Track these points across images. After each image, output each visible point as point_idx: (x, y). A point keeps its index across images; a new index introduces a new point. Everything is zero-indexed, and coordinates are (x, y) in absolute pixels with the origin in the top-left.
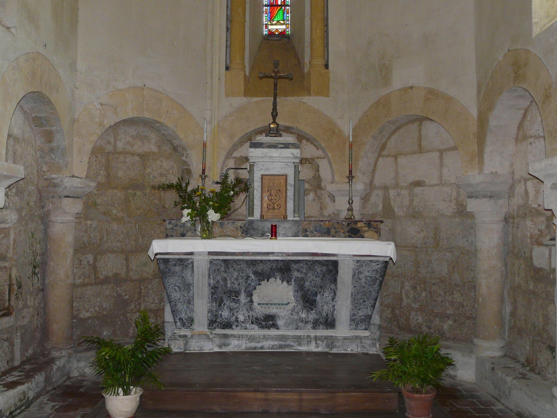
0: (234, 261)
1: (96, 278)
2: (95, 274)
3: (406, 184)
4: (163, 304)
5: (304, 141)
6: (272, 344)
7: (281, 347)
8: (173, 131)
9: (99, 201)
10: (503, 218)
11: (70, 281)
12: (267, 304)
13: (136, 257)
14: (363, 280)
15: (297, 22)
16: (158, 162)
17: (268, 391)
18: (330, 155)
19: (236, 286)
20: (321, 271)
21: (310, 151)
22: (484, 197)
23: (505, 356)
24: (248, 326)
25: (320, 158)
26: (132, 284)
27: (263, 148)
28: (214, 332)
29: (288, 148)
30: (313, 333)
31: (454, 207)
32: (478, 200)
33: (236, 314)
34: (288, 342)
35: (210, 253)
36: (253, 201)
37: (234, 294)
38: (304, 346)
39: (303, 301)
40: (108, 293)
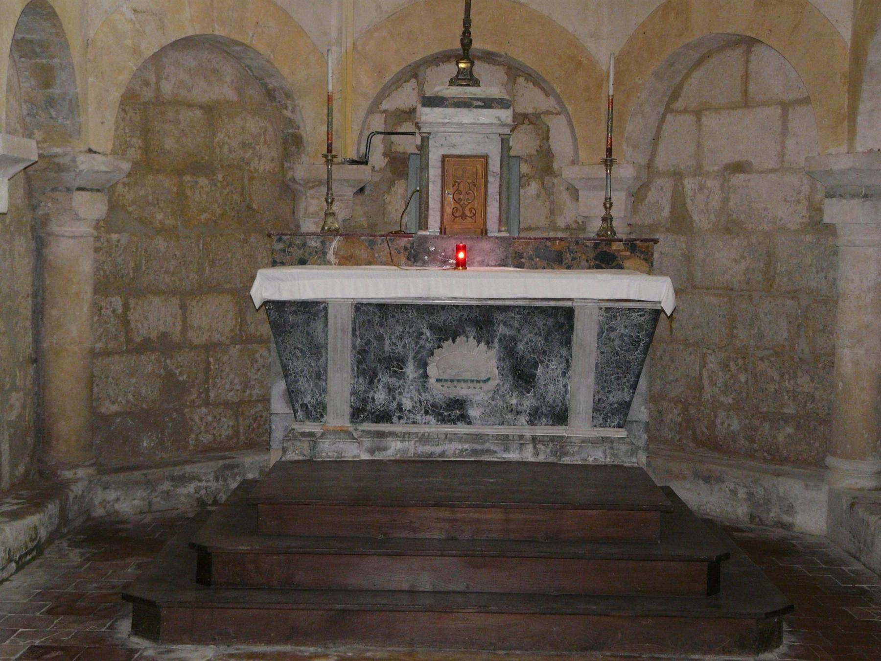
1: (129, 340)
2: (127, 333)
3: (716, 168)
4: (248, 392)
5: (521, 80)
6: (460, 447)
7: (474, 452)
8: (268, 61)
11: (87, 345)
12: (452, 381)
13: (200, 304)
14: (617, 342)
16: (238, 121)
17: (454, 506)
18: (570, 108)
19: (400, 349)
20: (545, 325)
21: (531, 99)
22: (854, 196)
24: (418, 417)
25: (552, 113)
26: (193, 354)
27: (446, 106)
28: (361, 428)
29: (490, 107)
30: (528, 432)
31: (804, 213)
32: (844, 201)
33: (398, 397)
34: (487, 446)
36: (427, 202)
37: (395, 364)
38: (514, 452)
39: (514, 377)
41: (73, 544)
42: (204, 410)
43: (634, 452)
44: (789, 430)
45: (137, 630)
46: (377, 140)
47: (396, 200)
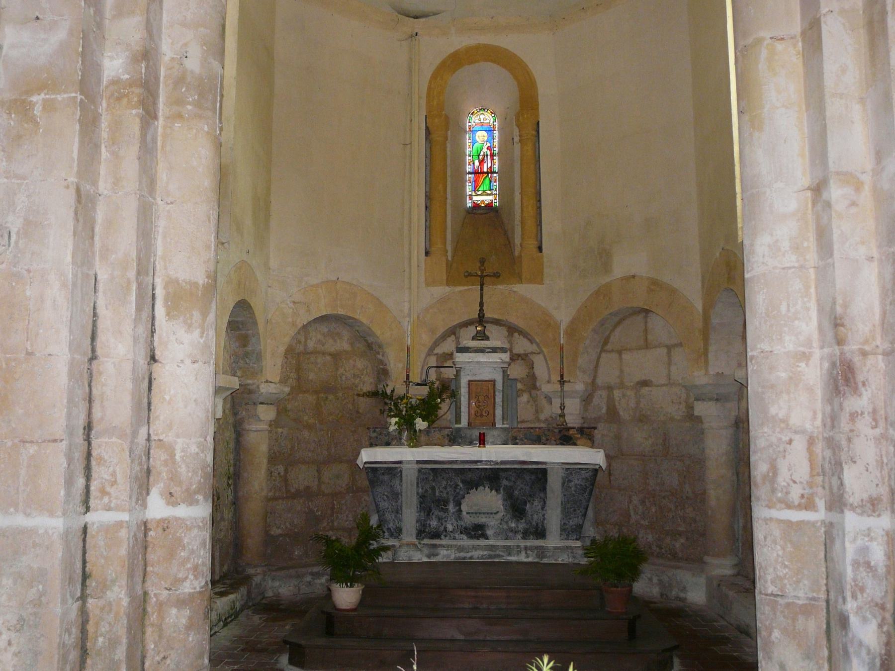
0: (443, 470)
5: (516, 334)
7: (490, 556)
9: (289, 407)
10: (733, 422)
11: (264, 493)
12: (476, 513)
14: (573, 488)
15: (506, 191)
16: (351, 361)
19: (445, 495)
22: (711, 399)
23: (738, 574)
24: (456, 535)
28: (422, 542)
31: (684, 409)
34: (497, 552)
35: (418, 462)
37: (442, 503)
40: (299, 508)
41: (256, 612)
44: (682, 540)
45: (292, 662)
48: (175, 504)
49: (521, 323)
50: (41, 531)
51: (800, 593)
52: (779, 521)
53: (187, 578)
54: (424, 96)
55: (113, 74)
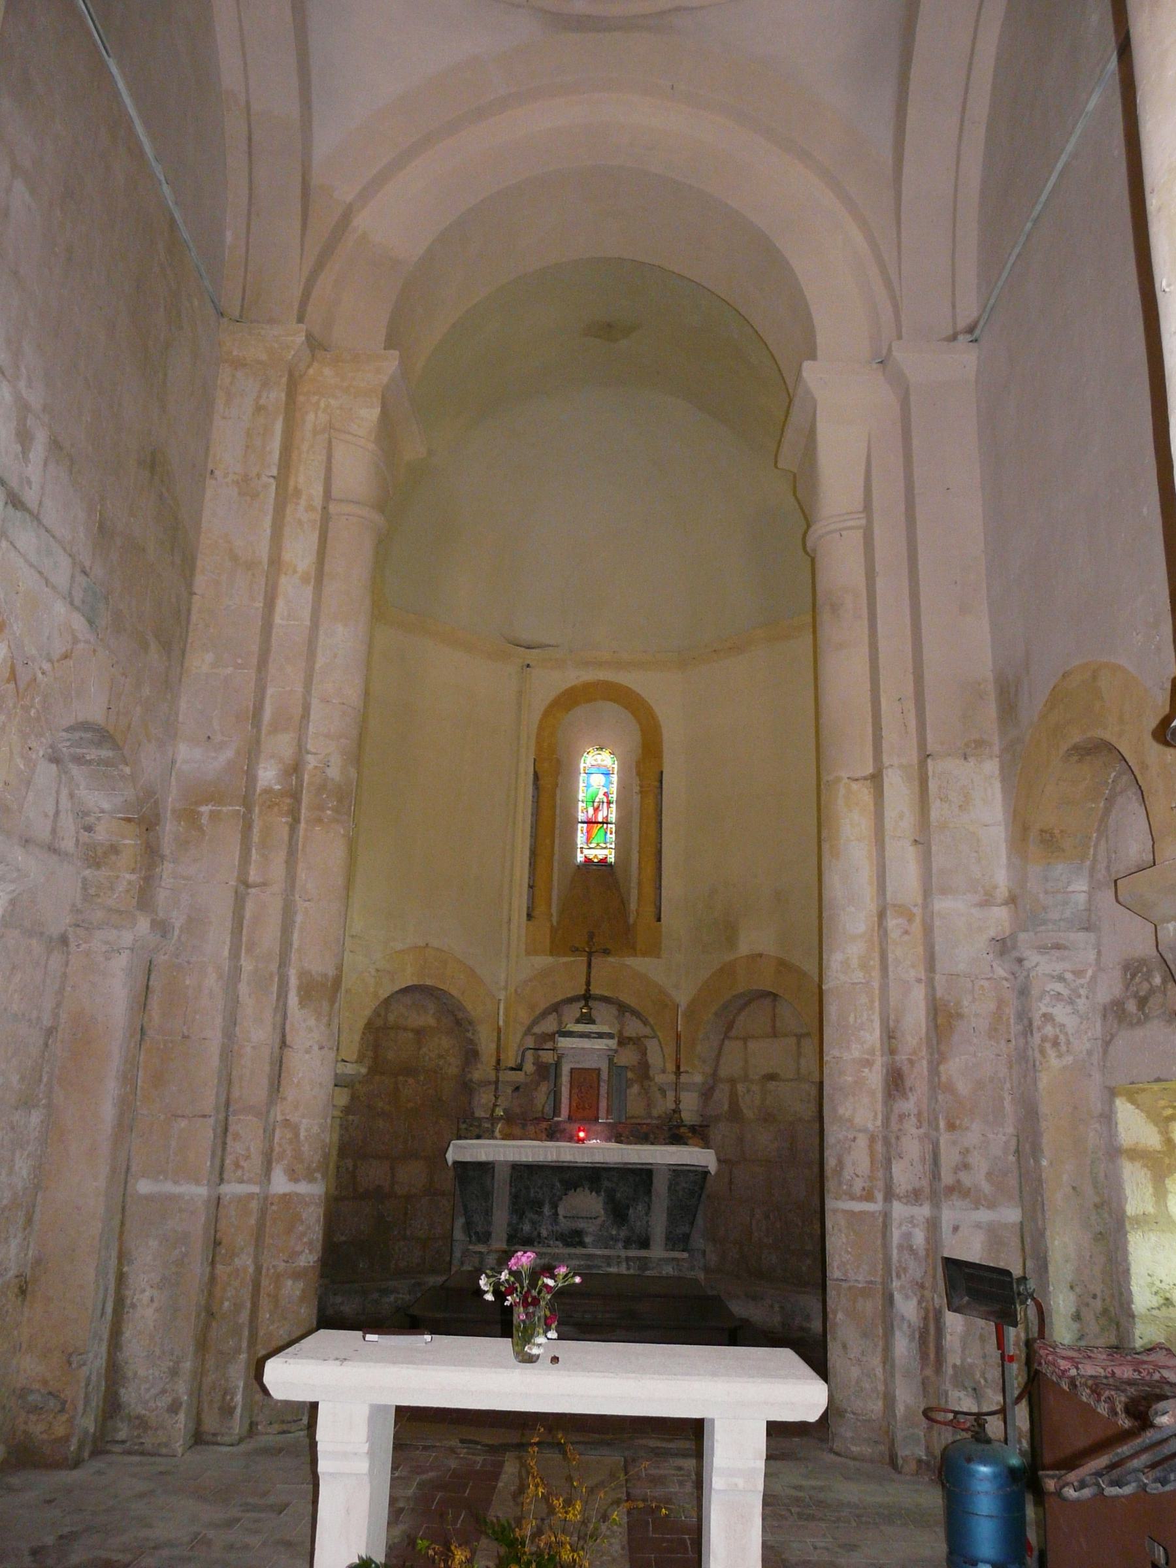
30: (623, 1253)
34: (596, 1262)
37: (537, 1205)
42: (402, 1243)
43: (692, 1268)
44: (809, 1262)
46: (529, 1054)
47: (541, 1096)
48: (296, 1181)
49: (631, 1001)
50: (187, 1198)
51: (860, 1277)
52: (845, 1212)
53: (303, 1251)
54: (533, 738)
55: (266, 783)
